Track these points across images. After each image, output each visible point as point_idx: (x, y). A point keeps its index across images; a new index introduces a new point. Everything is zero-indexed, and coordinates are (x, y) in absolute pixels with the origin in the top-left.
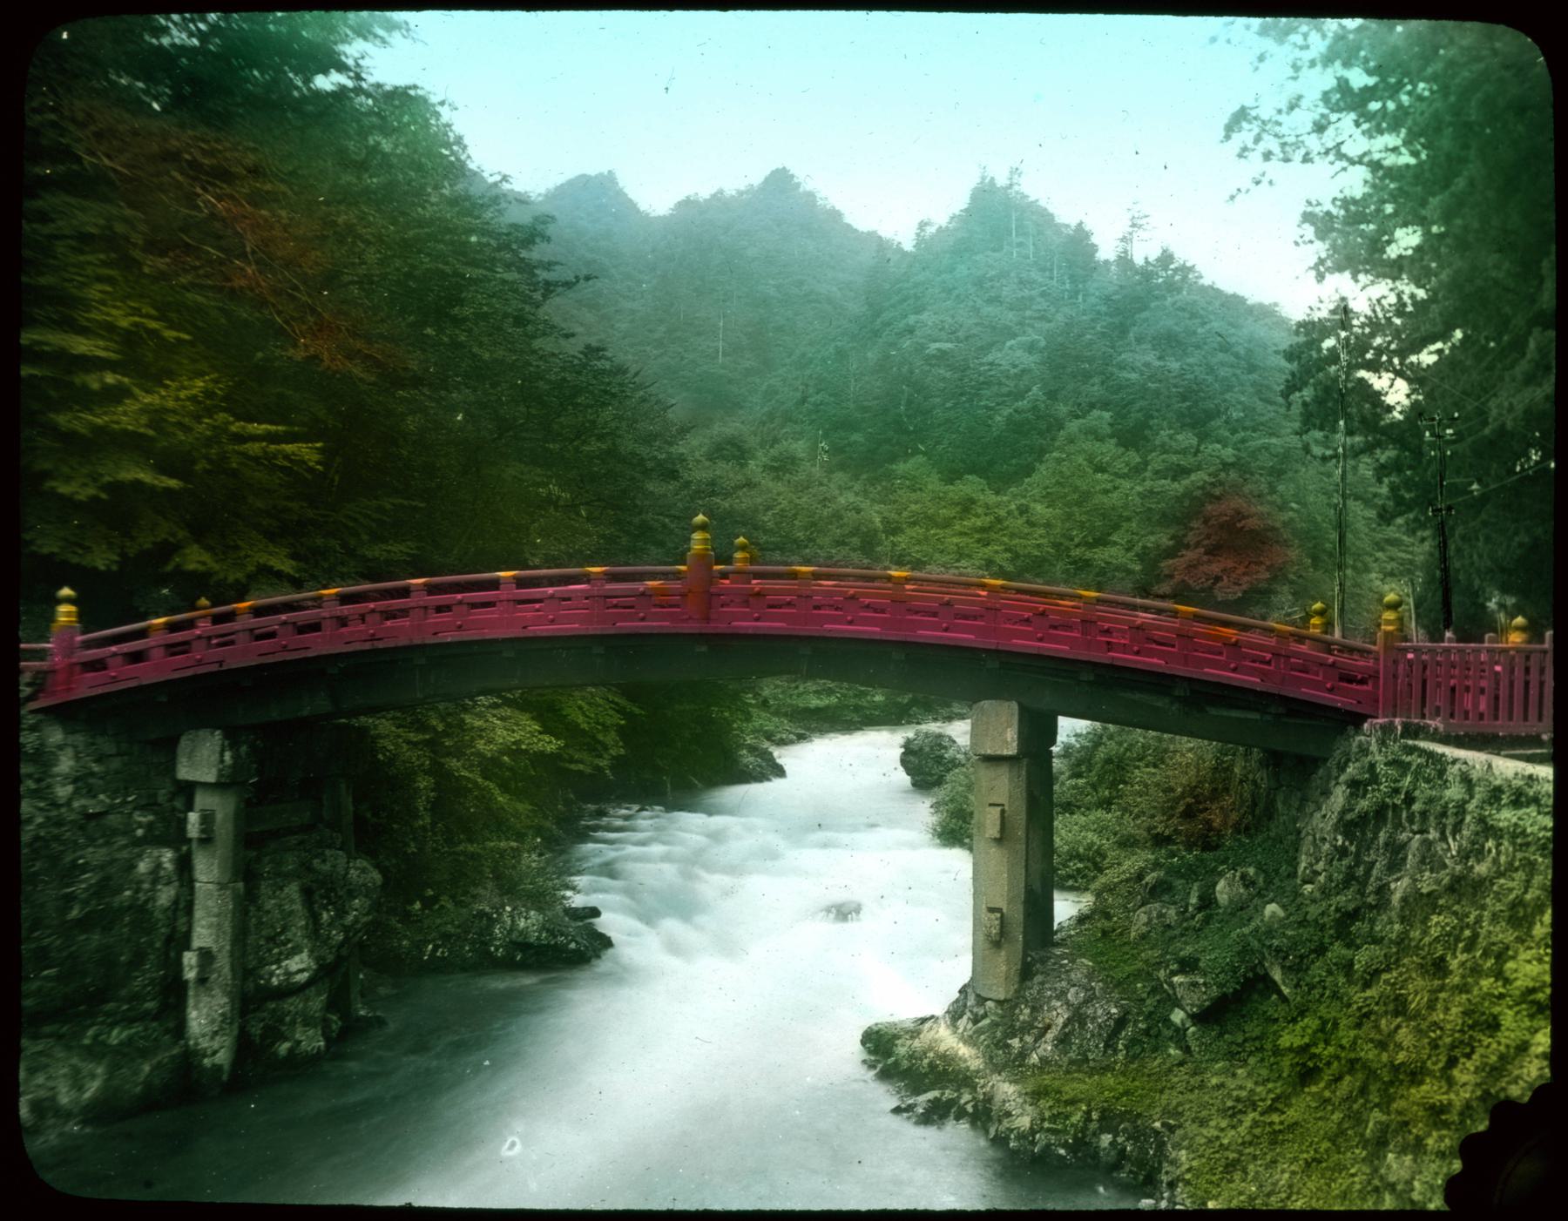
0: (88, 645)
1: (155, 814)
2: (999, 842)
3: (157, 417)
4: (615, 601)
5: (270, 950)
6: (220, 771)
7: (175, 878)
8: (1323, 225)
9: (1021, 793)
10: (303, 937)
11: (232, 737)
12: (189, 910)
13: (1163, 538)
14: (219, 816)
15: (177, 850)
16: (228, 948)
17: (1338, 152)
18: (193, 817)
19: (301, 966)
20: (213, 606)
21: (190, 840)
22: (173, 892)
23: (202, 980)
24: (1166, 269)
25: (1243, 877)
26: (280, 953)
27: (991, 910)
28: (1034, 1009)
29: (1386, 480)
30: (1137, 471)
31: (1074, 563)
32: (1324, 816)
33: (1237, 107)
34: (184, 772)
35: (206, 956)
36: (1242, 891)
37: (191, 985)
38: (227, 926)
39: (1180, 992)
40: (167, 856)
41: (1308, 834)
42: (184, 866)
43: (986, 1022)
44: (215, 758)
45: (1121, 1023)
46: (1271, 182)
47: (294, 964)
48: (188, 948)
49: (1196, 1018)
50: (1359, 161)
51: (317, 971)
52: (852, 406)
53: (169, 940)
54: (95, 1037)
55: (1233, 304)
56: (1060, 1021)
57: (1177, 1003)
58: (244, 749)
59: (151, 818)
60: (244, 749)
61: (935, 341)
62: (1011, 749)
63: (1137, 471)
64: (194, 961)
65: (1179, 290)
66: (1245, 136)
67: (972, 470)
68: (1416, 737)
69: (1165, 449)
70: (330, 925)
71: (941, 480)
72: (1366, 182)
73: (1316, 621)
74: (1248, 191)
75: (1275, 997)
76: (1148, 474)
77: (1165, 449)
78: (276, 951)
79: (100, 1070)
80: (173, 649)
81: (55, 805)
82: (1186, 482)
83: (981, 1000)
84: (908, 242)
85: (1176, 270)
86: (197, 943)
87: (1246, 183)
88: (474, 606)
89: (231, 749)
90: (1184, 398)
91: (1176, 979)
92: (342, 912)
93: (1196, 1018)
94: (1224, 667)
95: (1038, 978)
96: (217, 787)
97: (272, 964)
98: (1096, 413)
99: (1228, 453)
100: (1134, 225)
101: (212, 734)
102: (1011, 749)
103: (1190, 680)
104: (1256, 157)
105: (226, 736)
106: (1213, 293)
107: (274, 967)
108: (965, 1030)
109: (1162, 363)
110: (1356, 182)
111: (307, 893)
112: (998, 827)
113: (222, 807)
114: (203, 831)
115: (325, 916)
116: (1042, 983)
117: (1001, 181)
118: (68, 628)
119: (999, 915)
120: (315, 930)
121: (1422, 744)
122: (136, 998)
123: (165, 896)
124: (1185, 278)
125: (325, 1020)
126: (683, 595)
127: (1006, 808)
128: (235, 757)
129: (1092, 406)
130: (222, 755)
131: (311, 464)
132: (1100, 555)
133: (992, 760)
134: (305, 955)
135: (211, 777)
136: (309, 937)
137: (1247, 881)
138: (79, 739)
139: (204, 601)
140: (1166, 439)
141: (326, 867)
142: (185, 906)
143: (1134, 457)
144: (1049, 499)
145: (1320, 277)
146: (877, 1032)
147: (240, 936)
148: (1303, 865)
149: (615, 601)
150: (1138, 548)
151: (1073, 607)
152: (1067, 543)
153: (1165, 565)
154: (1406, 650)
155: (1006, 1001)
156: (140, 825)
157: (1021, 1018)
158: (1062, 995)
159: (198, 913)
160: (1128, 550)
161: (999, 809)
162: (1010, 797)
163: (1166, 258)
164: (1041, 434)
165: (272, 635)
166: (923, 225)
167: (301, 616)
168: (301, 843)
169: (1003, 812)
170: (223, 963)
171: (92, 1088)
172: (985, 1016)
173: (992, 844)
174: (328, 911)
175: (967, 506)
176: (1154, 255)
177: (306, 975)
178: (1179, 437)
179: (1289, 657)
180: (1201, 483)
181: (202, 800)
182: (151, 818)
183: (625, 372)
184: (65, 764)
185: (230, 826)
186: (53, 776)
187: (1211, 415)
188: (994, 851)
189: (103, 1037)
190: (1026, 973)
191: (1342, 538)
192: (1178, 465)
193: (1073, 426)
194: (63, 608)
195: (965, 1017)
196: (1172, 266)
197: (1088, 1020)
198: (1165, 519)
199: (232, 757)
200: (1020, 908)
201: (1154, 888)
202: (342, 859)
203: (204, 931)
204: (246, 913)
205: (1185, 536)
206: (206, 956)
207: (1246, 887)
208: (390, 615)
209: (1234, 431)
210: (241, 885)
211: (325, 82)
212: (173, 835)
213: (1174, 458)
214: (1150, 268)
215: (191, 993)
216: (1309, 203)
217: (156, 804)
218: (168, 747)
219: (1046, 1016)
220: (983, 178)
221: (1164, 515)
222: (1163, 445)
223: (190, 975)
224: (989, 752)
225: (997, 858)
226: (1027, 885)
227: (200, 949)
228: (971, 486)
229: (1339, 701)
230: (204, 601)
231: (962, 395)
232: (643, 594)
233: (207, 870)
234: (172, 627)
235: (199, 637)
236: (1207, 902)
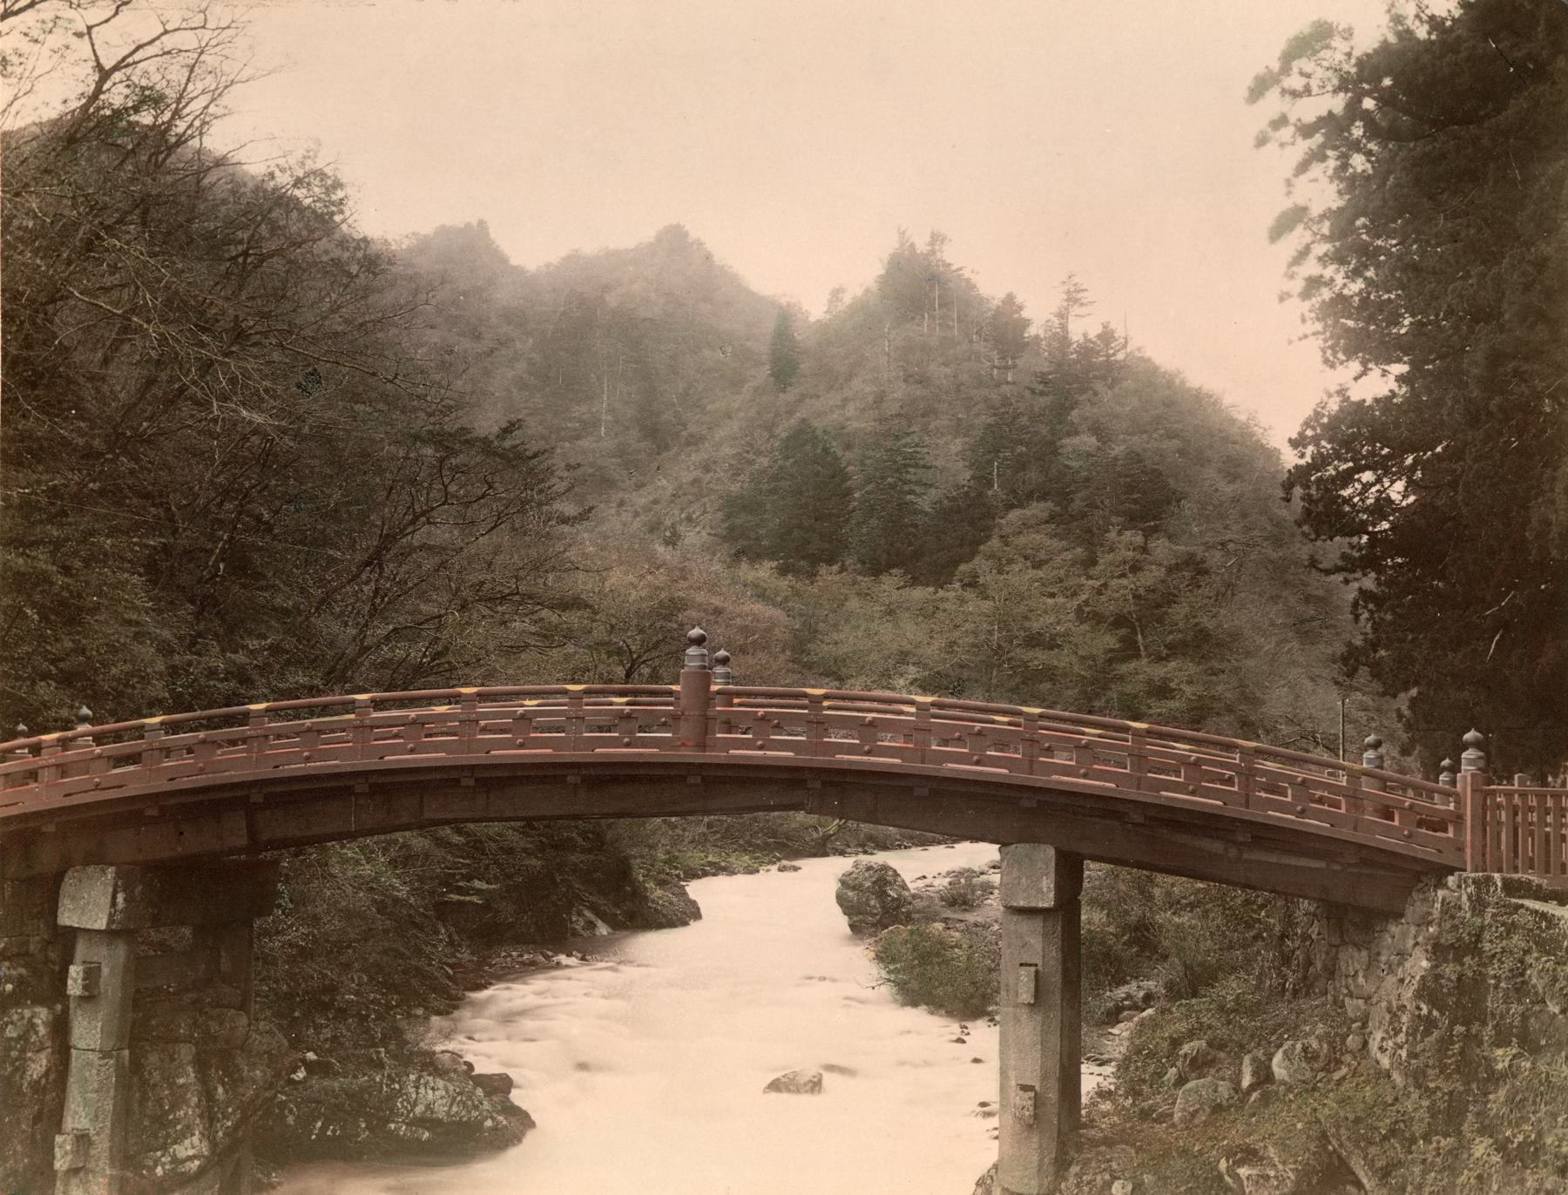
1: (26, 966)
6: (111, 916)
7: (49, 1044)
9: (1055, 953)
14: (105, 971)
18: (75, 971)
27: (1024, 1088)
34: (68, 917)
35: (83, 1140)
40: (42, 1015)
42: (61, 1028)
47: (183, 1150)
55: (1198, 397)
86: (69, 1123)
89: (124, 891)
96: (110, 934)
101: (103, 871)
103: (1361, 846)
106: (884, 281)
107: (159, 1153)
111: (201, 1064)
113: (111, 961)
114: (85, 987)
117: (922, 246)
119: (1032, 1094)
120: (210, 1116)
127: (1040, 968)
130: (114, 897)
134: (195, 1139)
137: (1309, 1056)
161: (1033, 969)
163: (1107, 336)
166: (836, 294)
168: (194, 1002)
169: (1037, 972)
177: (197, 1163)
181: (81, 950)
185: (117, 981)
190: (1061, 1164)
191: (500, 456)
199: (125, 899)
201: (1194, 1061)
206: (83, 1140)
210: (126, 1053)
217: (27, 954)
220: (902, 244)
224: (1022, 903)
225: (1029, 1029)
229: (1427, 852)
233: (88, 1032)
236: (1264, 1076)
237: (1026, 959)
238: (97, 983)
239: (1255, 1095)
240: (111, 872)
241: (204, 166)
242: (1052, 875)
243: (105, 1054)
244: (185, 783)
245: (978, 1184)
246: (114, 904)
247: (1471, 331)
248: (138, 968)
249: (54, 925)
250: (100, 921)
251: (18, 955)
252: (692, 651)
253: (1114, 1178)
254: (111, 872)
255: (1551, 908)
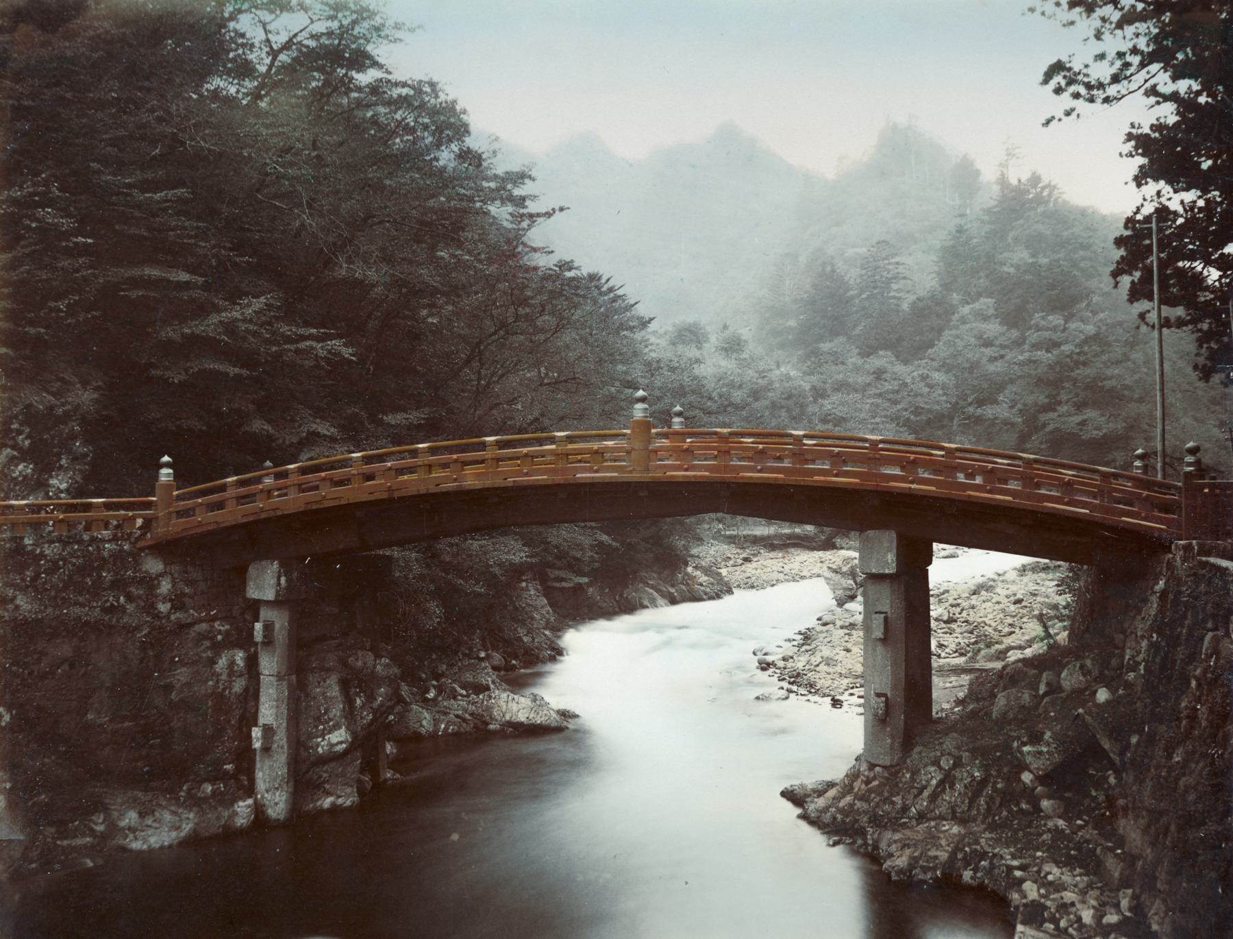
1: (231, 625)
4: (579, 457)
5: (317, 727)
6: (277, 591)
8: (1142, 143)
10: (341, 717)
11: (286, 568)
14: (277, 626)
15: (246, 651)
16: (285, 725)
18: (258, 626)
19: (340, 739)
20: (275, 466)
21: (256, 644)
22: (244, 683)
23: (266, 749)
24: (1035, 187)
25: (1082, 667)
26: (324, 729)
27: (878, 695)
29: (1205, 346)
30: (1019, 343)
31: (969, 418)
32: (1143, 618)
33: (1055, 60)
34: (253, 593)
35: (268, 731)
36: (1081, 678)
37: (258, 752)
39: (1029, 759)
40: (239, 657)
41: (1132, 633)
42: (252, 663)
43: (876, 783)
44: (273, 581)
45: (983, 782)
46: (1078, 115)
48: (256, 725)
51: (352, 743)
52: (787, 299)
56: (934, 782)
57: (1026, 768)
58: (295, 574)
59: (227, 627)
60: (295, 574)
61: (853, 247)
62: (891, 569)
63: (1019, 343)
64: (259, 734)
65: (1047, 202)
66: (1059, 79)
67: (885, 347)
68: (1209, 554)
69: (1038, 329)
70: (361, 708)
71: (859, 354)
73: (1138, 463)
74: (1060, 120)
75: (1105, 762)
76: (1026, 347)
77: (1038, 329)
78: (321, 727)
79: (191, 816)
80: (241, 499)
83: (872, 766)
84: (830, 174)
85: (1043, 188)
86: (261, 721)
91: (1026, 749)
92: (371, 698)
93: (1041, 779)
95: (917, 749)
96: (276, 603)
97: (318, 737)
98: (982, 300)
99: (1090, 329)
100: (1008, 155)
102: (891, 569)
104: (1066, 96)
107: (319, 740)
108: (859, 789)
109: (1034, 260)
110: (1168, 113)
111: (345, 685)
112: (882, 630)
113: (280, 620)
115: (358, 701)
116: (920, 753)
118: (168, 487)
119: (883, 699)
120: (350, 713)
121: (1212, 560)
123: (238, 686)
124: (1050, 195)
125: (359, 781)
126: (628, 452)
127: (889, 615)
129: (979, 295)
130: (279, 578)
131: (347, 356)
132: (989, 411)
136: (346, 718)
138: (175, 568)
139: (268, 463)
140: (1039, 320)
142: (252, 694)
143: (1015, 334)
144: (945, 367)
145: (1139, 185)
146: (792, 791)
148: (1127, 657)
149: (579, 457)
150: (1019, 406)
151: (815, 445)
152: (961, 403)
153: (1043, 418)
155: (892, 766)
156: (220, 632)
157: (904, 780)
158: (936, 763)
160: (1011, 407)
161: (882, 616)
162: (891, 607)
163: (1035, 179)
164: (938, 316)
169: (886, 619)
170: (281, 738)
171: (187, 828)
172: (875, 778)
173: (879, 643)
174: (360, 697)
175: (879, 374)
176: (1025, 177)
177: (344, 746)
178: (1051, 318)
179: (568, 455)
180: (1068, 353)
181: (265, 614)
182: (227, 627)
183: (599, 279)
184: (165, 586)
185: (285, 633)
186: (156, 597)
187: (1074, 300)
188: (880, 648)
189: (193, 791)
192: (1050, 340)
193: (966, 310)
194: (164, 471)
195: (860, 780)
196: (1040, 185)
197: (956, 781)
198: (1040, 382)
199: (287, 581)
202: (370, 657)
203: (267, 712)
205: (1058, 394)
206: (268, 731)
207: (1084, 675)
210: (294, 677)
212: (243, 639)
213: (1047, 334)
214: (1022, 187)
215: (258, 758)
216: (1133, 126)
218: (241, 574)
222: (1037, 325)
223: (257, 745)
226: (907, 675)
227: (264, 725)
228: (883, 359)
230: (268, 463)
231: (875, 288)
232: (596, 452)
233: (269, 665)
234: (241, 483)
235: (262, 491)
237: (880, 608)
238: (273, 635)
239: (1046, 699)
240: (276, 564)
242: (895, 551)
245: (856, 760)
246: (279, 584)
247: (1166, 98)
248: (297, 624)
249: (244, 597)
250: (270, 595)
251: (226, 617)
252: (639, 406)
253: (942, 755)
254: (276, 564)
255: (1225, 563)
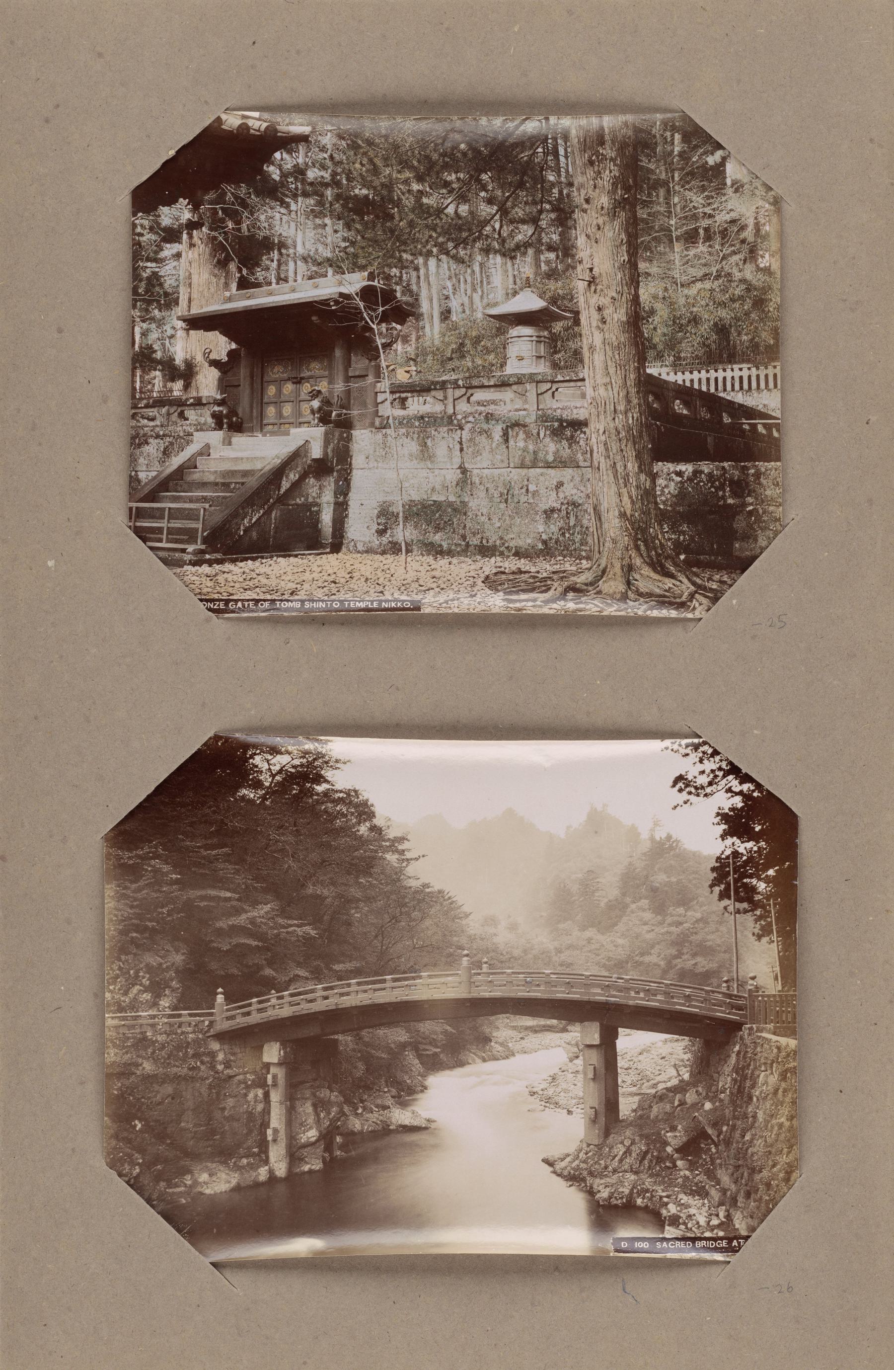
0: (227, 1010)
2: (594, 1079)
3: (252, 921)
11: (284, 1045)
12: (269, 1113)
13: (674, 952)
14: (279, 1076)
17: (729, 790)
18: (269, 1077)
23: (275, 1141)
24: (669, 841)
27: (591, 1108)
28: (610, 1149)
30: (661, 923)
33: (678, 774)
35: (276, 1131)
38: (284, 1119)
39: (670, 1140)
40: (260, 1092)
42: (267, 1095)
49: (677, 1151)
50: (737, 794)
53: (262, 1125)
54: (235, 1163)
56: (621, 1153)
62: (597, 1042)
65: (675, 849)
66: (681, 785)
72: (372, 805)
73: (724, 985)
81: (217, 1072)
82: (681, 927)
83: (589, 1145)
86: (272, 1126)
87: (681, 803)
88: (375, 990)
90: (679, 894)
92: (329, 1113)
93: (677, 1151)
94: (683, 1005)
95: (612, 1135)
96: (279, 1064)
102: (597, 1042)
105: (281, 1044)
111: (315, 1106)
113: (280, 1073)
117: (599, 809)
118: (222, 1005)
120: (318, 1121)
122: (249, 1148)
123: (260, 1107)
124: (677, 845)
128: (285, 1053)
132: (647, 959)
133: (590, 1046)
134: (314, 1130)
135: (276, 1061)
138: (226, 1047)
139: (273, 991)
141: (322, 1095)
142: (267, 1111)
143: (659, 918)
145: (723, 840)
147: (289, 1123)
150: (662, 956)
154: (758, 996)
158: (622, 1143)
159: (273, 1114)
163: (669, 837)
165: (299, 1004)
166: (568, 827)
167: (309, 996)
170: (282, 1135)
175: (589, 940)
176: (664, 836)
181: (273, 1070)
184: (221, 1057)
188: (592, 1084)
190: (607, 1133)
200: (603, 1106)
204: (291, 1113)
206: (276, 1131)
208: (342, 995)
209: (701, 906)
210: (288, 1103)
211: (320, 788)
219: (615, 1151)
221: (673, 942)
223: (270, 1138)
228: (590, 933)
241: (685, 849)
243: (281, 1103)
244: (365, 1003)
250: (276, 1061)
252: (465, 959)
